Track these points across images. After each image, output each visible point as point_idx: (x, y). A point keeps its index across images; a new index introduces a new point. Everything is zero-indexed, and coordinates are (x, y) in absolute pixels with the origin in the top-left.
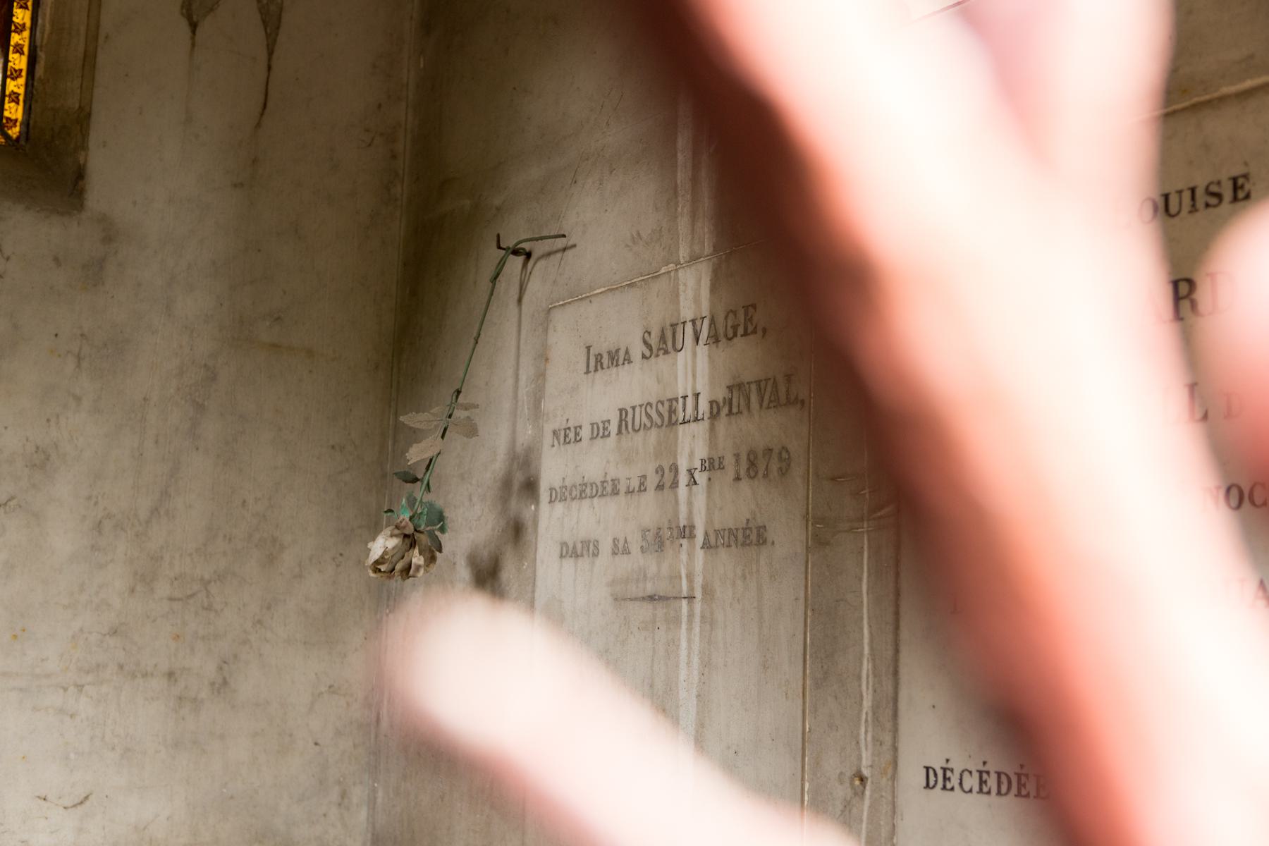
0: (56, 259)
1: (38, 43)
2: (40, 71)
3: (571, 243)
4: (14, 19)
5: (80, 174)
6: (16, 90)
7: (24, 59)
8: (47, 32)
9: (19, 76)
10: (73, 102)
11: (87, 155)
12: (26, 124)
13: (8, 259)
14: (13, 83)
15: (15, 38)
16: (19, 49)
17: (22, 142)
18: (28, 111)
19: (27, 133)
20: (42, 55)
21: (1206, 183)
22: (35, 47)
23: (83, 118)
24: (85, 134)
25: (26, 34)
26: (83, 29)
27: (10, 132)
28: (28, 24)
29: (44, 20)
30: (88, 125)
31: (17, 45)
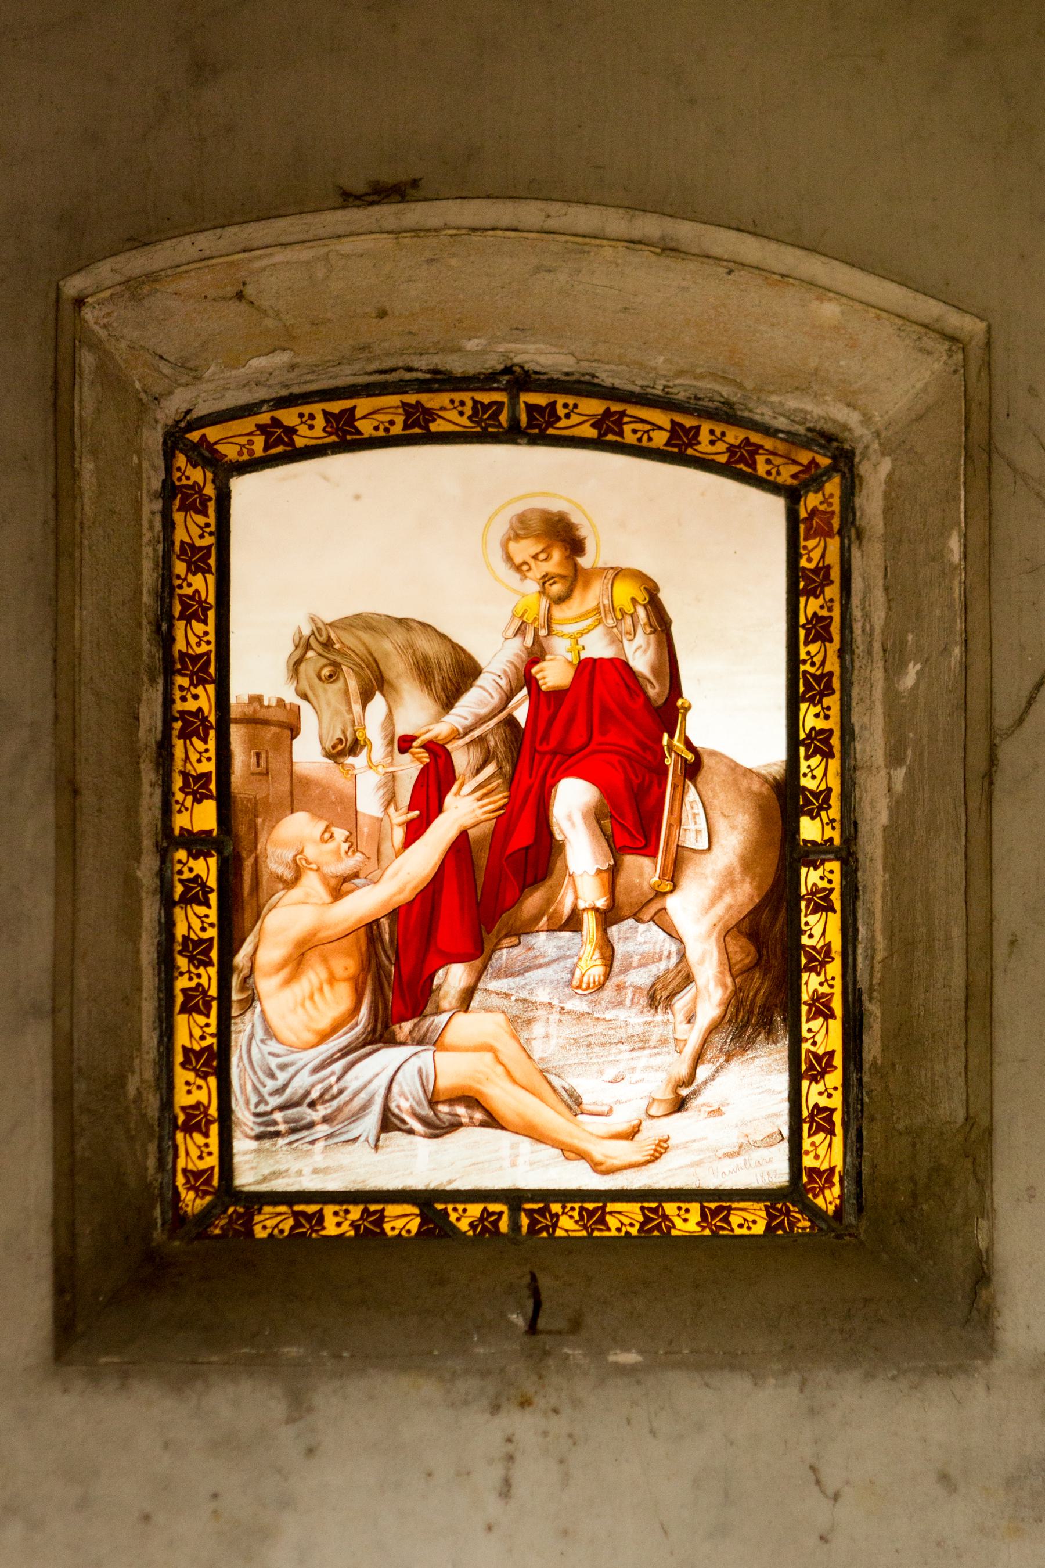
0: (944, 1478)
1: (863, 984)
2: (872, 1047)
3: (283, 1168)
4: (805, 940)
5: (982, 1274)
6: (823, 1102)
7: (836, 1026)
8: (880, 956)
9: (829, 1067)
10: (951, 1109)
11: (992, 1227)
12: (855, 1175)
13: (836, 1497)
14: (816, 1088)
15: (811, 984)
16: (821, 1009)
17: (850, 1219)
18: (855, 1146)
19: (859, 1196)
20: (873, 1009)
21: (643, 1111)
22: (858, 994)
23: (976, 1143)
24: (983, 1182)
25: (834, 969)
26: (957, 932)
27: (820, 1202)
28: (837, 946)
29: (871, 929)
30: (990, 1157)
31: (817, 997)
